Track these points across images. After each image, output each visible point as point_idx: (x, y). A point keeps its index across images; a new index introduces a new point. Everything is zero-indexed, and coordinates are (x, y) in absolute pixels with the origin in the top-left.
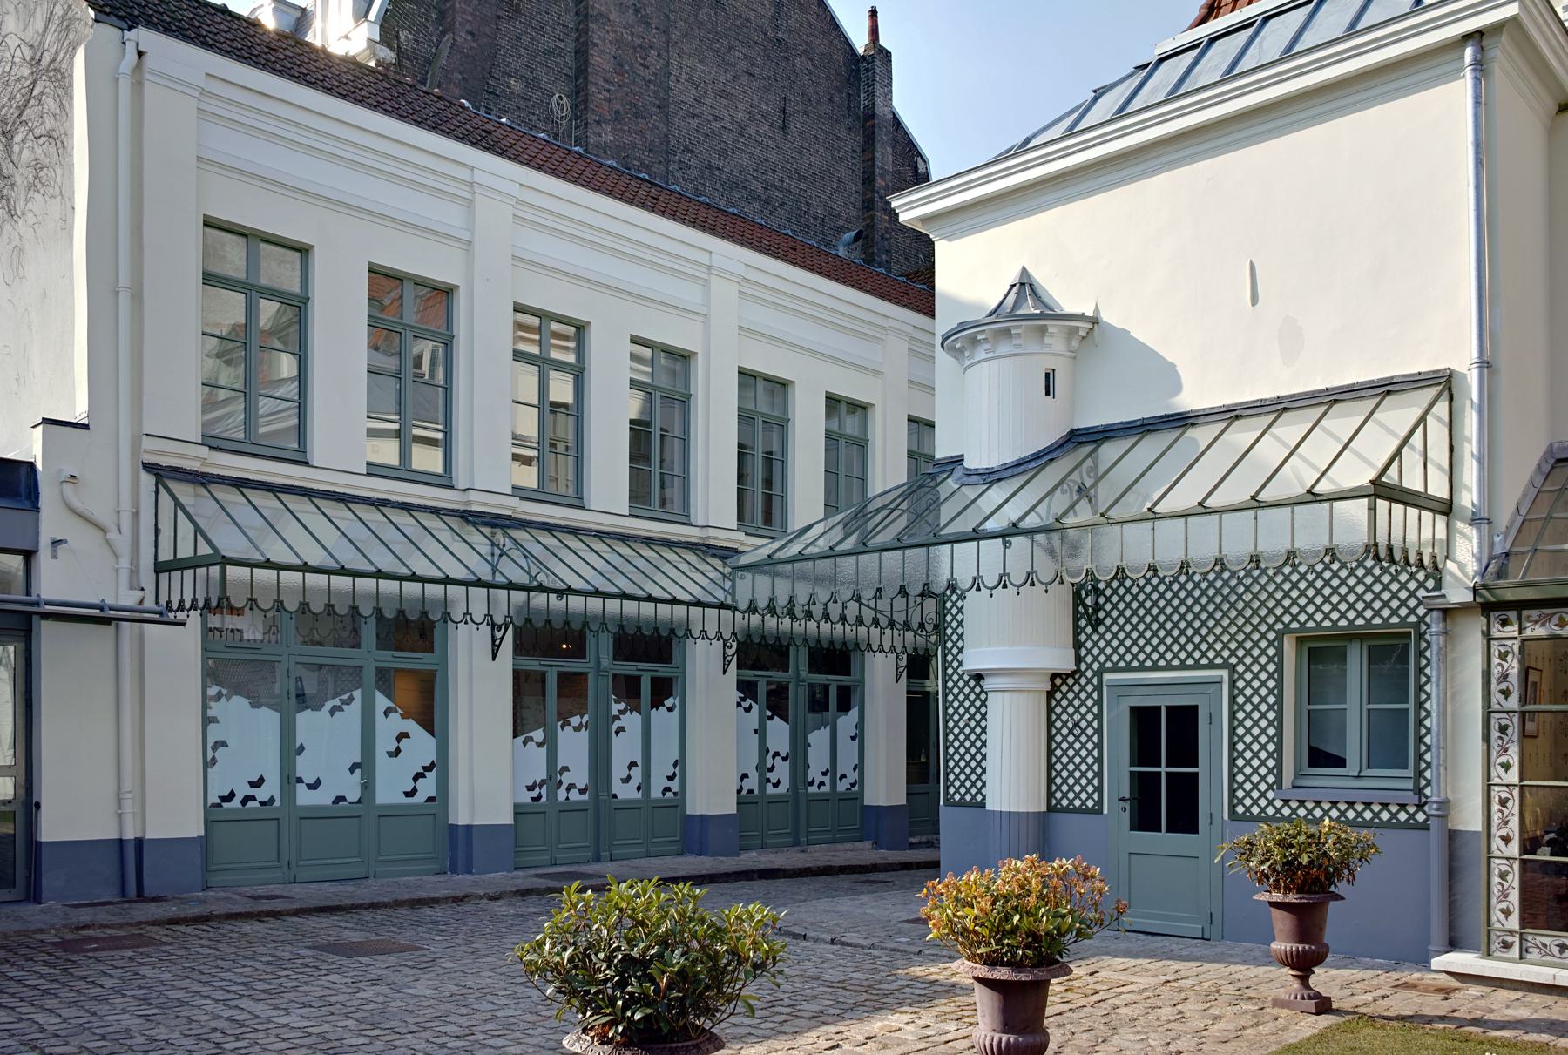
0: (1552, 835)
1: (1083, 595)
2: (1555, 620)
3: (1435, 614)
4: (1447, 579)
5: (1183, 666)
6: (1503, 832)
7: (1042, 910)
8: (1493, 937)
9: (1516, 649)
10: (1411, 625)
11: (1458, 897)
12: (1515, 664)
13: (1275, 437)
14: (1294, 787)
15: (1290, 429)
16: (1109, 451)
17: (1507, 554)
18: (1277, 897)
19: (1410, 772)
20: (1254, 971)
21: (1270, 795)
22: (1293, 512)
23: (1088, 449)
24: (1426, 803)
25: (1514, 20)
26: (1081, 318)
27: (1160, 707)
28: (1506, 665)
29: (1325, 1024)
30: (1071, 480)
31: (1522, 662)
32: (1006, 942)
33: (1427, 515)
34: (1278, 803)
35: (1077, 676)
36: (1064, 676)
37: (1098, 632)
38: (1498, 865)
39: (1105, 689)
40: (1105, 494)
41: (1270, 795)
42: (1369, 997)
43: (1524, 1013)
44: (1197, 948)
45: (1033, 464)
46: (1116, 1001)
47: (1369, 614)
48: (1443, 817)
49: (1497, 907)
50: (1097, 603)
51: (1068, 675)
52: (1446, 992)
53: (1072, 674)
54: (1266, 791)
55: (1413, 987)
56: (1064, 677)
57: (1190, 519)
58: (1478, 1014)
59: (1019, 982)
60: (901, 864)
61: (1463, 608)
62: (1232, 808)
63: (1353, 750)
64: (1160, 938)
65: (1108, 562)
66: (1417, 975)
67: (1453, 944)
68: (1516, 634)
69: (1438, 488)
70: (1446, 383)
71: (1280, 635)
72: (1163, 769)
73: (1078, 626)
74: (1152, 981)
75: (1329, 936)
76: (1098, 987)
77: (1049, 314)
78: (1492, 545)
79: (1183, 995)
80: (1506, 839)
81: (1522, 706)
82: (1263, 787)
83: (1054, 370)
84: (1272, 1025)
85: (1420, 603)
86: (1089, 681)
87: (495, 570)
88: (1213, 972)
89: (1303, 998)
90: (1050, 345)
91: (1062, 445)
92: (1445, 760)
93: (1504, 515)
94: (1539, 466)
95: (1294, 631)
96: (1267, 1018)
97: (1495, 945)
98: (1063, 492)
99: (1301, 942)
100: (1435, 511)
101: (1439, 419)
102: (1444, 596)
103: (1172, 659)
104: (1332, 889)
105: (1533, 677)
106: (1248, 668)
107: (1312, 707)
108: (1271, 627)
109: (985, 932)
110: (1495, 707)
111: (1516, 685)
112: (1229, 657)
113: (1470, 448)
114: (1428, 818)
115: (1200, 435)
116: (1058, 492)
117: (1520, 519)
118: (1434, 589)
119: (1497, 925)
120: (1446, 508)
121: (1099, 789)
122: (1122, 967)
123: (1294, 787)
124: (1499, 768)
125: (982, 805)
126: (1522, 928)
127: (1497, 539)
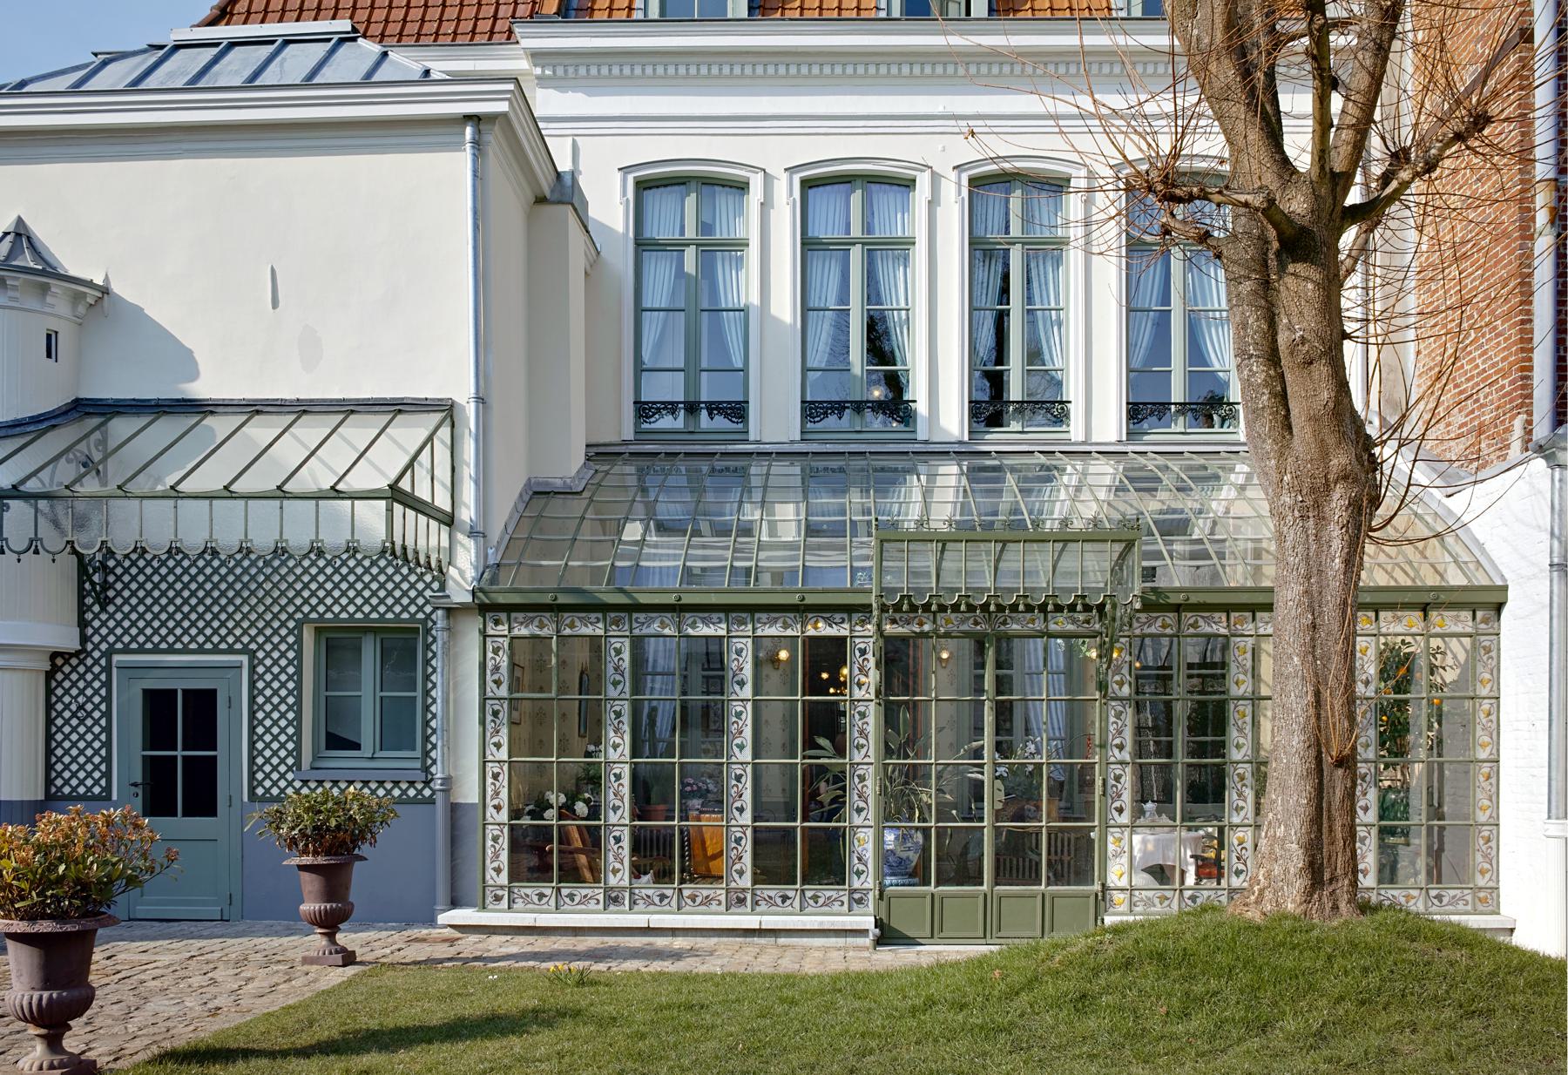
0: (531, 807)
1: (91, 571)
2: (536, 622)
3: (440, 612)
4: (450, 583)
5: (201, 650)
6: (496, 802)
7: (91, 858)
8: (488, 892)
9: (506, 645)
10: (419, 621)
11: (459, 861)
12: (505, 658)
13: (294, 436)
14: (312, 768)
15: (310, 431)
16: (121, 427)
17: (498, 565)
18: (307, 860)
19: (418, 753)
20: (276, 941)
21: (290, 776)
22: (317, 505)
23: (96, 421)
24: (432, 780)
25: (504, 115)
26: (89, 284)
27: (176, 691)
28: (498, 659)
29: (353, 972)
30: (78, 451)
31: (511, 657)
32: (49, 893)
33: (433, 524)
34: (297, 784)
36: (66, 656)
37: (107, 612)
38: (492, 831)
39: (115, 671)
40: (116, 472)
41: (290, 776)
42: (388, 951)
43: (514, 950)
44: (219, 928)
45: (32, 428)
46: (142, 977)
47: (382, 609)
48: (446, 791)
49: (490, 866)
50: (105, 581)
51: (71, 655)
52: (451, 942)
53: (77, 654)
54: (286, 772)
55: (424, 940)
57: (215, 502)
58: (479, 954)
59: (66, 934)
61: (463, 608)
62: (252, 790)
63: (368, 732)
64: (176, 924)
65: (123, 541)
66: (425, 931)
67: (455, 903)
68: (506, 633)
69: (443, 502)
70: (447, 410)
71: (300, 624)
72: (179, 753)
73: (84, 604)
74: (177, 958)
75: (354, 896)
76: (119, 967)
77: (49, 272)
78: (486, 557)
79: (212, 966)
80: (498, 808)
82: (283, 768)
83: (56, 333)
84: (303, 979)
85: (427, 602)
86: (96, 662)
88: (237, 946)
89: (331, 953)
90: (52, 306)
91: (65, 413)
92: (448, 741)
93: (496, 532)
94: (521, 495)
95: (314, 621)
96: (298, 974)
97: (489, 899)
98: (69, 461)
99: (328, 901)
100: (440, 521)
101: (443, 442)
102: (448, 597)
103: (190, 643)
104: (356, 851)
105: (518, 673)
106: (268, 655)
107: (329, 693)
108: (291, 616)
109: (25, 885)
110: (490, 694)
111: (506, 674)
112: (249, 643)
113: (468, 471)
114: (434, 792)
115: (219, 425)
116: (63, 460)
117: (508, 537)
118: (438, 591)
119: (491, 882)
120: (449, 520)
121: (107, 775)
122: (141, 949)
123: (312, 768)
124: (492, 747)
126: (510, 882)
127: (490, 551)
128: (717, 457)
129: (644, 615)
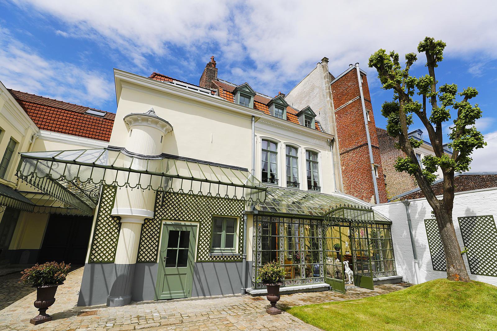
35: (153, 220)
48: (245, 259)
51: (150, 219)
53: (152, 220)
56: (149, 220)
60: (203, 288)
81: (263, 234)
87: (36, 167)
125: (113, 262)
128: (31, 141)
129: (265, 217)
